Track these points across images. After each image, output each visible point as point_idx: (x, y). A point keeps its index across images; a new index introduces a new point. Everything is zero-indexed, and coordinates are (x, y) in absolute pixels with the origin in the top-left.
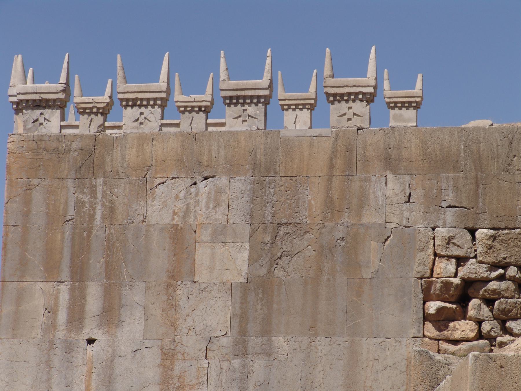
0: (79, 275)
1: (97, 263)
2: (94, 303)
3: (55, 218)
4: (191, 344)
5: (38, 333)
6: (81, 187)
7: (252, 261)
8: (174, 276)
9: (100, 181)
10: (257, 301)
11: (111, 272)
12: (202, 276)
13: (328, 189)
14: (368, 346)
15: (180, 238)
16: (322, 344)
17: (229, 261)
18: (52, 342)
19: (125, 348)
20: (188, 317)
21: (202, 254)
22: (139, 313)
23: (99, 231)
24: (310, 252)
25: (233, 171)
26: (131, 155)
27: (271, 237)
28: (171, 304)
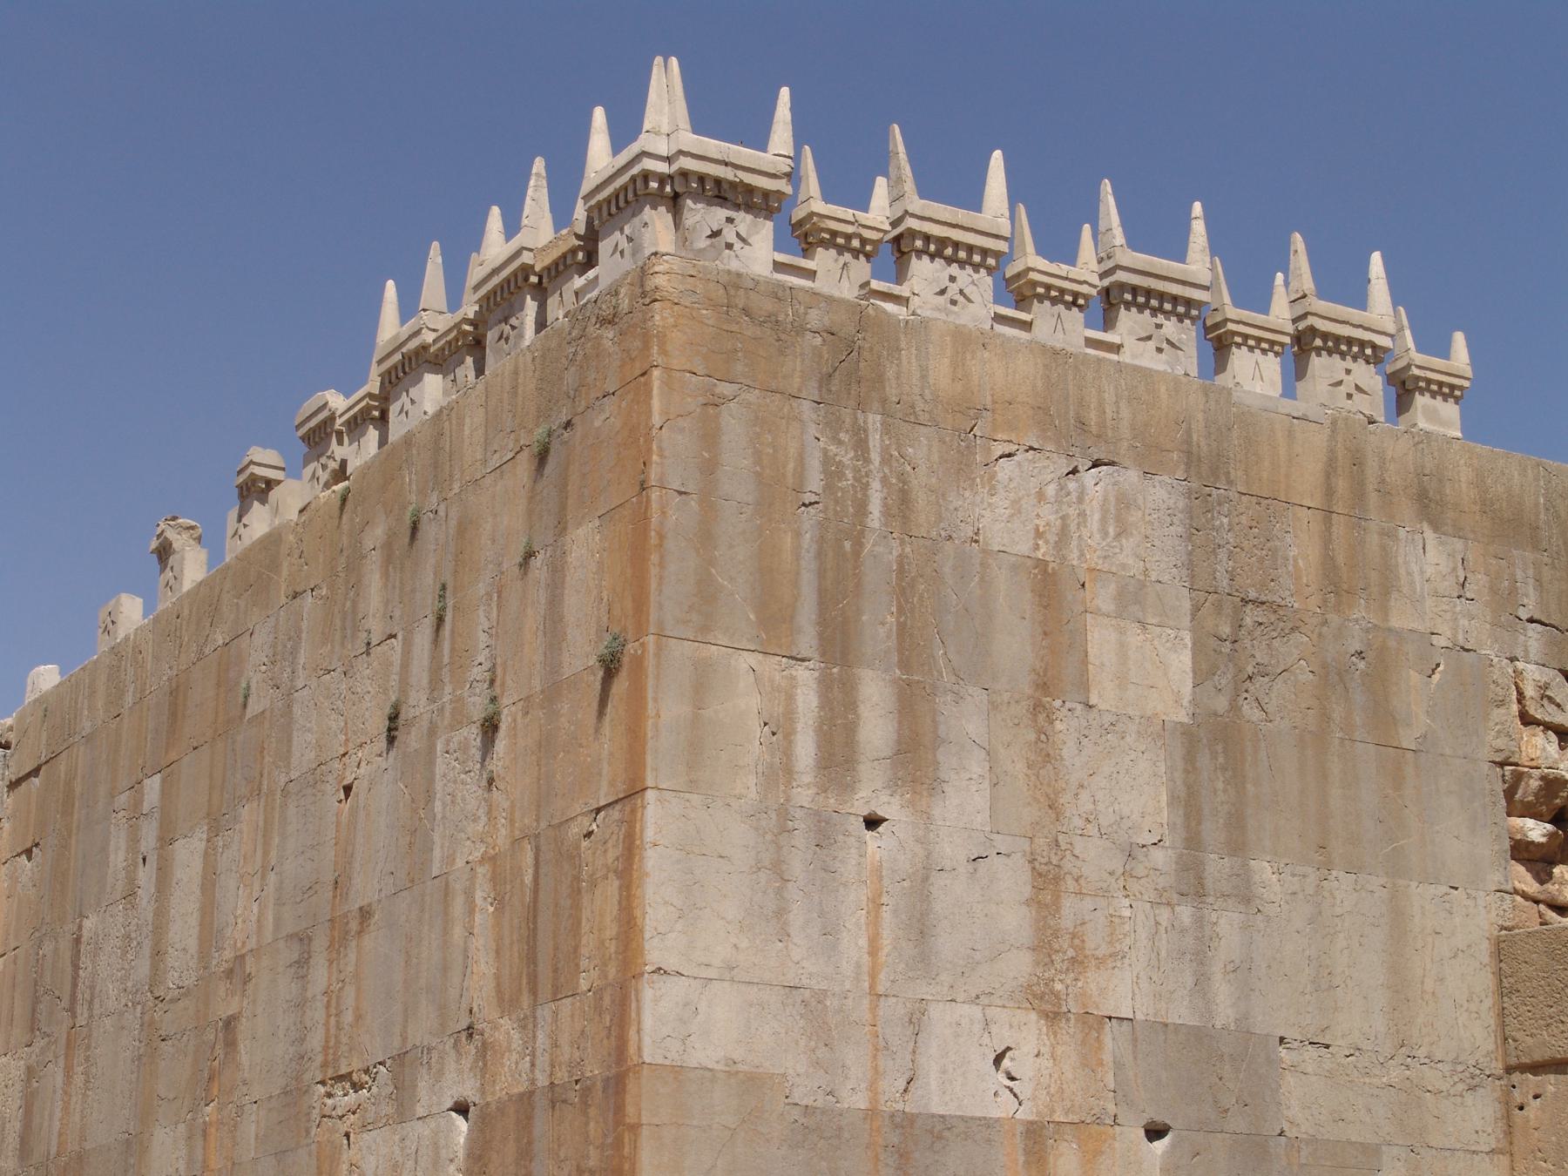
0: (839, 649)
1: (877, 625)
2: (876, 729)
4: (1092, 858)
5: (748, 786)
6: (832, 426)
7: (1202, 675)
8: (1045, 685)
9: (874, 420)
12: (1104, 695)
13: (1327, 541)
16: (1342, 885)
17: (1148, 669)
18: (784, 814)
19: (953, 850)
21: (1101, 640)
22: (977, 765)
23: (882, 549)
26: (941, 371)
27: (1234, 614)
28: (1044, 755)
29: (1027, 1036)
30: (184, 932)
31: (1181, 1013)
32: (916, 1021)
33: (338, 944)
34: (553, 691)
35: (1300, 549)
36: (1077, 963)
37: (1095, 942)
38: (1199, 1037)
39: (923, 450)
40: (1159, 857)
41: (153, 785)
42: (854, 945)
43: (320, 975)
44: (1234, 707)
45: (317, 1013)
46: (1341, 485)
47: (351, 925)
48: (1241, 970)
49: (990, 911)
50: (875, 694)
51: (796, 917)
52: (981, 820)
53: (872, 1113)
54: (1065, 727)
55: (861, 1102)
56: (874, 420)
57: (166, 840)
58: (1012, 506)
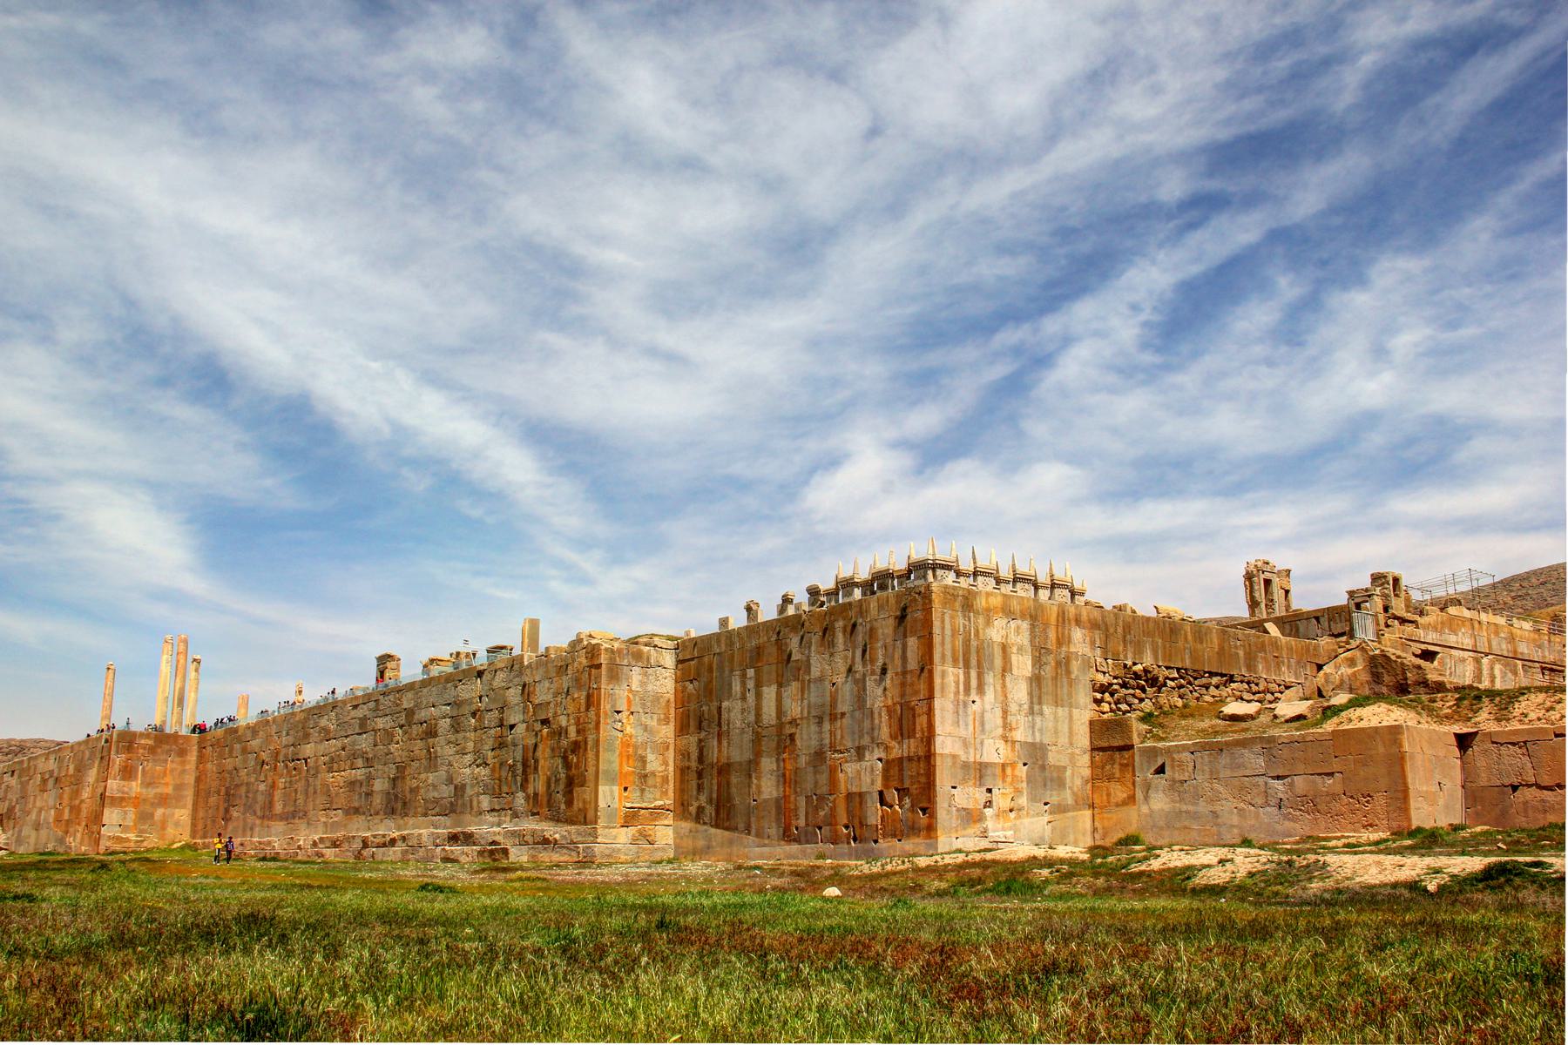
2: (974, 683)
4: (1013, 708)
7: (1033, 666)
8: (1004, 670)
11: (979, 665)
12: (1015, 671)
16: (1060, 710)
17: (1023, 665)
19: (988, 707)
21: (1014, 658)
25: (1023, 617)
27: (1039, 653)
28: (1004, 686)
31: (1030, 740)
35: (1052, 635)
38: (1033, 745)
39: (981, 620)
41: (751, 672)
42: (971, 728)
49: (994, 719)
50: (973, 674)
57: (758, 685)
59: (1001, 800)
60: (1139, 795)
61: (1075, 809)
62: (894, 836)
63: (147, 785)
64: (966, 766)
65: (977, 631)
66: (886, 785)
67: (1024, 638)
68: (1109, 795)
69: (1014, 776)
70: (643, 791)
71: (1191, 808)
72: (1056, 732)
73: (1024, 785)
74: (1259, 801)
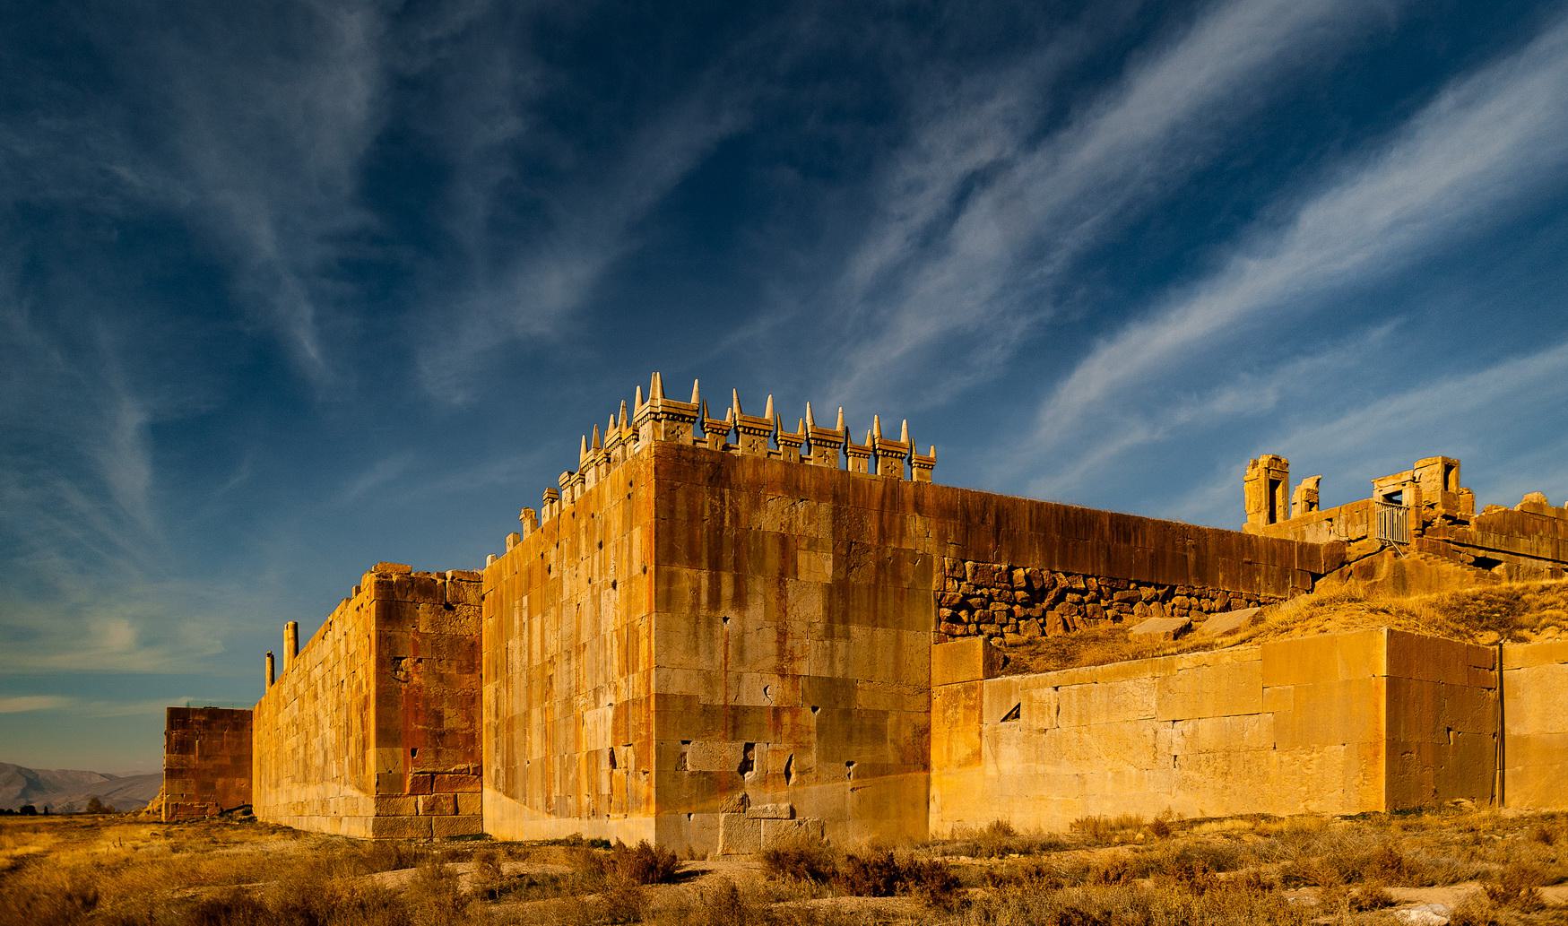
0: (715, 566)
1: (728, 558)
2: (727, 590)
3: (694, 516)
4: (797, 627)
5: (687, 610)
6: (713, 494)
7: (836, 567)
8: (783, 574)
9: (727, 491)
10: (840, 598)
11: (737, 565)
12: (802, 576)
13: (881, 520)
14: (908, 636)
15: (785, 543)
16: (880, 632)
17: (818, 567)
18: (697, 618)
19: (751, 627)
20: (806, 479)
21: (802, 558)
22: (760, 600)
23: (730, 533)
24: (872, 564)
25: (820, 496)
26: (749, 472)
27: (848, 552)
28: (782, 596)
29: (775, 684)
30: (536, 648)
31: (825, 674)
32: (739, 679)
33: (578, 654)
34: (630, 580)
35: (872, 525)
36: (792, 660)
37: (798, 653)
38: (831, 680)
39: (744, 502)
40: (819, 626)
41: (525, 599)
42: (720, 656)
43: (573, 663)
44: (847, 579)
45: (573, 675)
46: (887, 502)
47: (580, 649)
48: (846, 661)
49: (764, 644)
50: (727, 580)
51: (701, 649)
52: (761, 617)
53: (725, 706)
54: (790, 584)
55: (722, 703)
56: (727, 491)
57: (530, 617)
58: (770, 518)
59: (766, 756)
60: (986, 749)
61: (900, 770)
62: (622, 810)
63: (205, 756)
64: (707, 710)
65: (736, 517)
66: (616, 742)
67: (823, 530)
68: (949, 750)
69: (795, 726)
70: (438, 753)
71: (1050, 769)
72: (872, 662)
73: (813, 737)
74: (1145, 760)
